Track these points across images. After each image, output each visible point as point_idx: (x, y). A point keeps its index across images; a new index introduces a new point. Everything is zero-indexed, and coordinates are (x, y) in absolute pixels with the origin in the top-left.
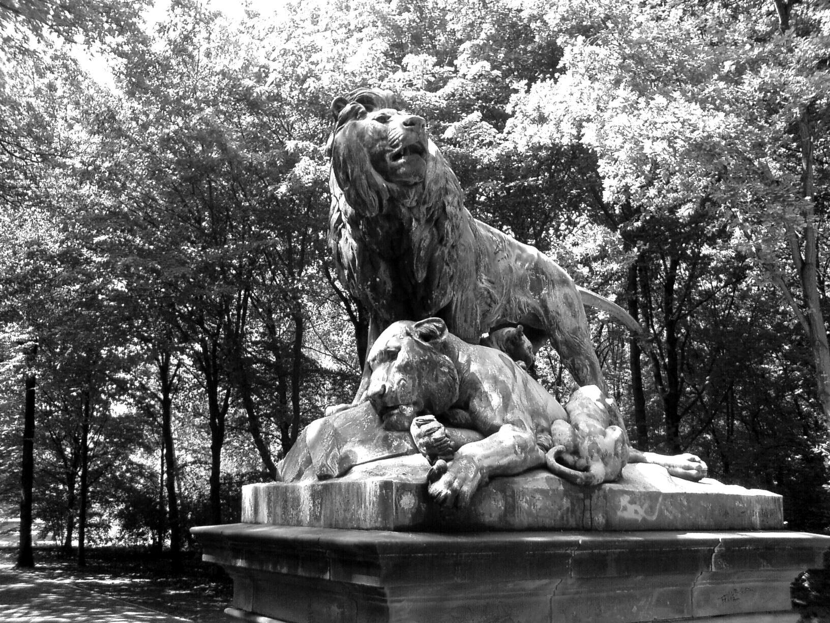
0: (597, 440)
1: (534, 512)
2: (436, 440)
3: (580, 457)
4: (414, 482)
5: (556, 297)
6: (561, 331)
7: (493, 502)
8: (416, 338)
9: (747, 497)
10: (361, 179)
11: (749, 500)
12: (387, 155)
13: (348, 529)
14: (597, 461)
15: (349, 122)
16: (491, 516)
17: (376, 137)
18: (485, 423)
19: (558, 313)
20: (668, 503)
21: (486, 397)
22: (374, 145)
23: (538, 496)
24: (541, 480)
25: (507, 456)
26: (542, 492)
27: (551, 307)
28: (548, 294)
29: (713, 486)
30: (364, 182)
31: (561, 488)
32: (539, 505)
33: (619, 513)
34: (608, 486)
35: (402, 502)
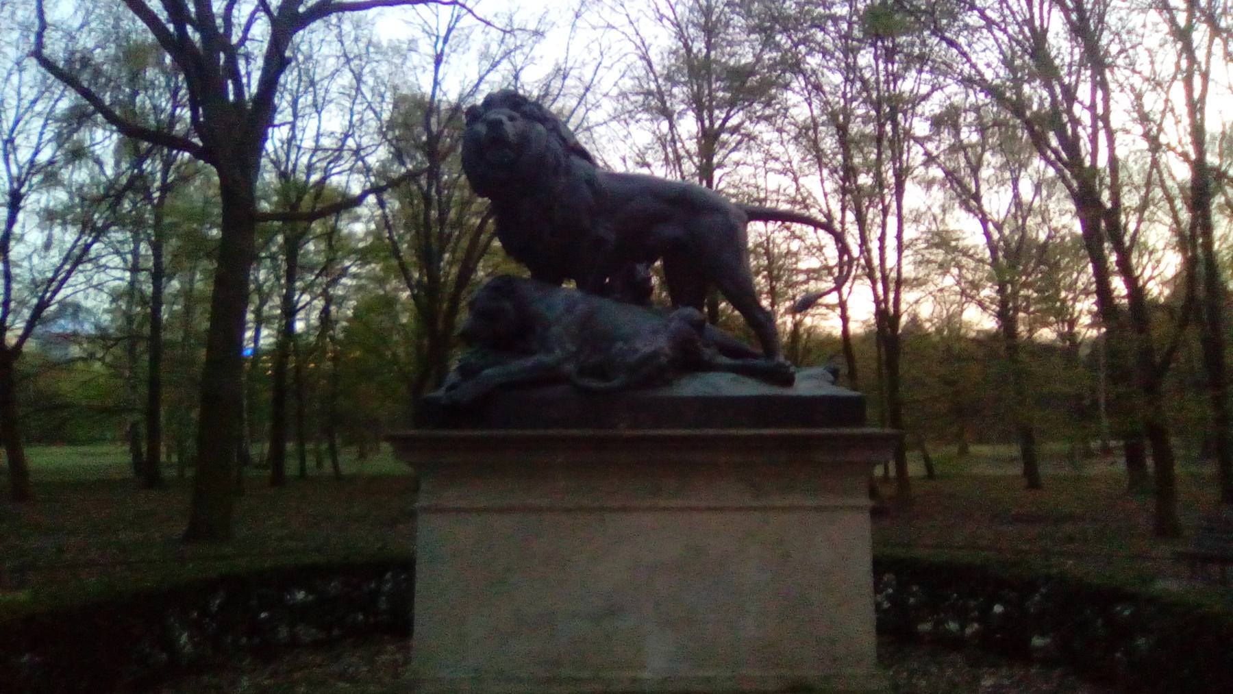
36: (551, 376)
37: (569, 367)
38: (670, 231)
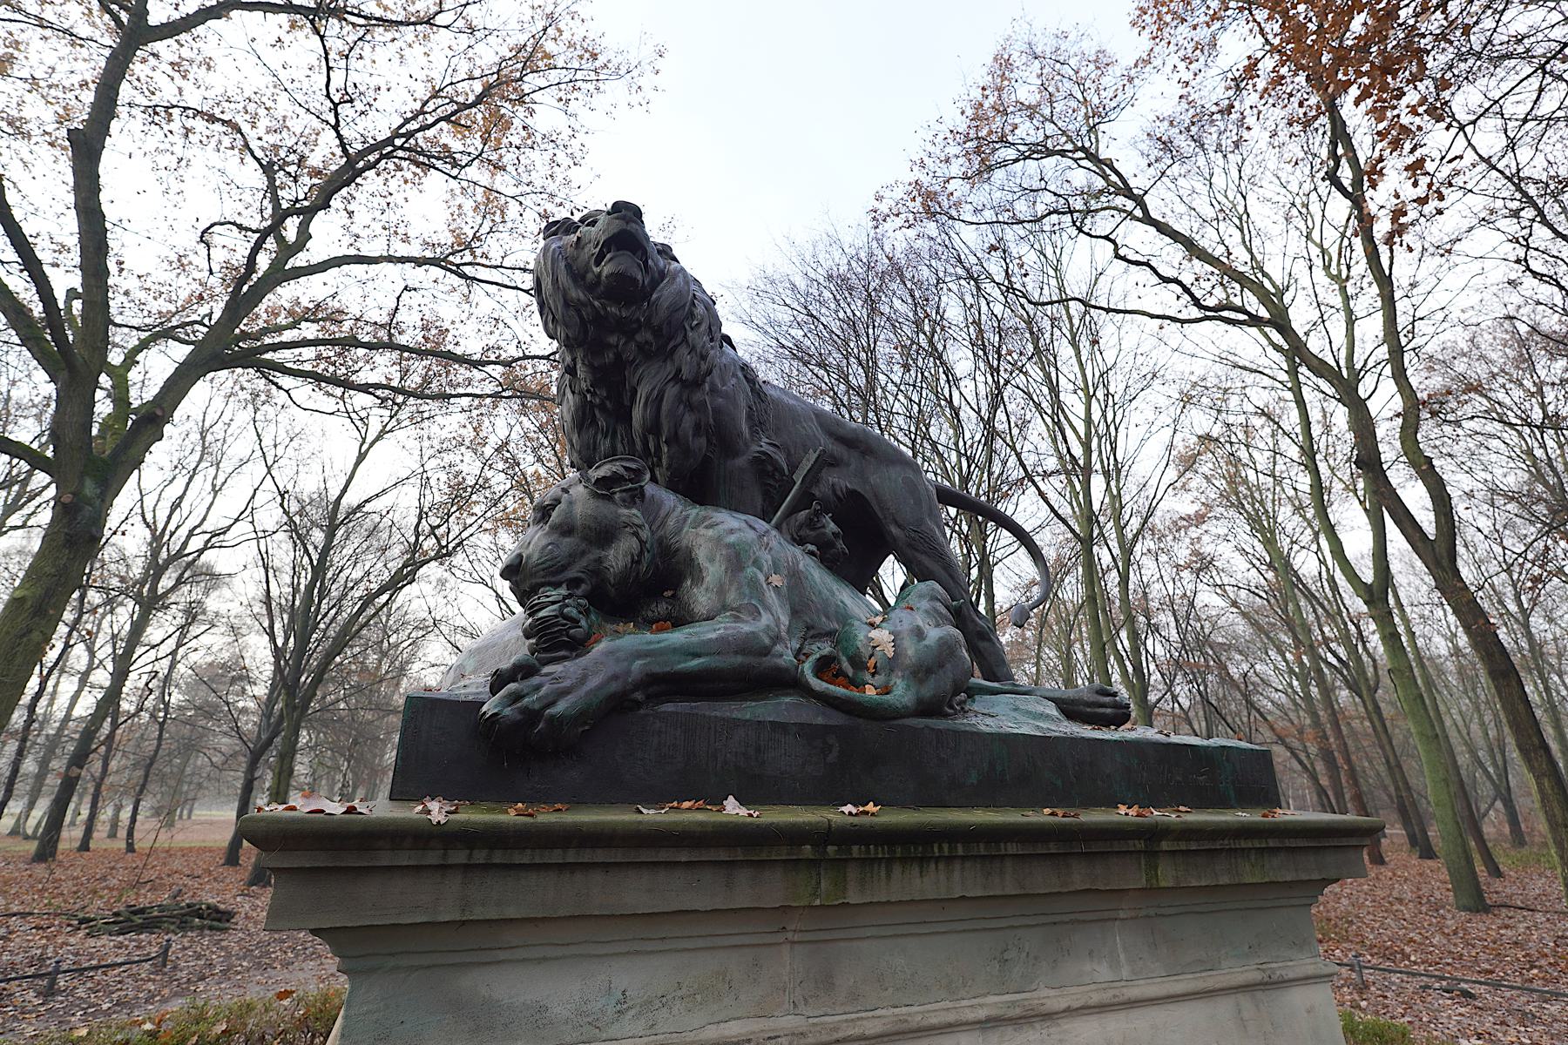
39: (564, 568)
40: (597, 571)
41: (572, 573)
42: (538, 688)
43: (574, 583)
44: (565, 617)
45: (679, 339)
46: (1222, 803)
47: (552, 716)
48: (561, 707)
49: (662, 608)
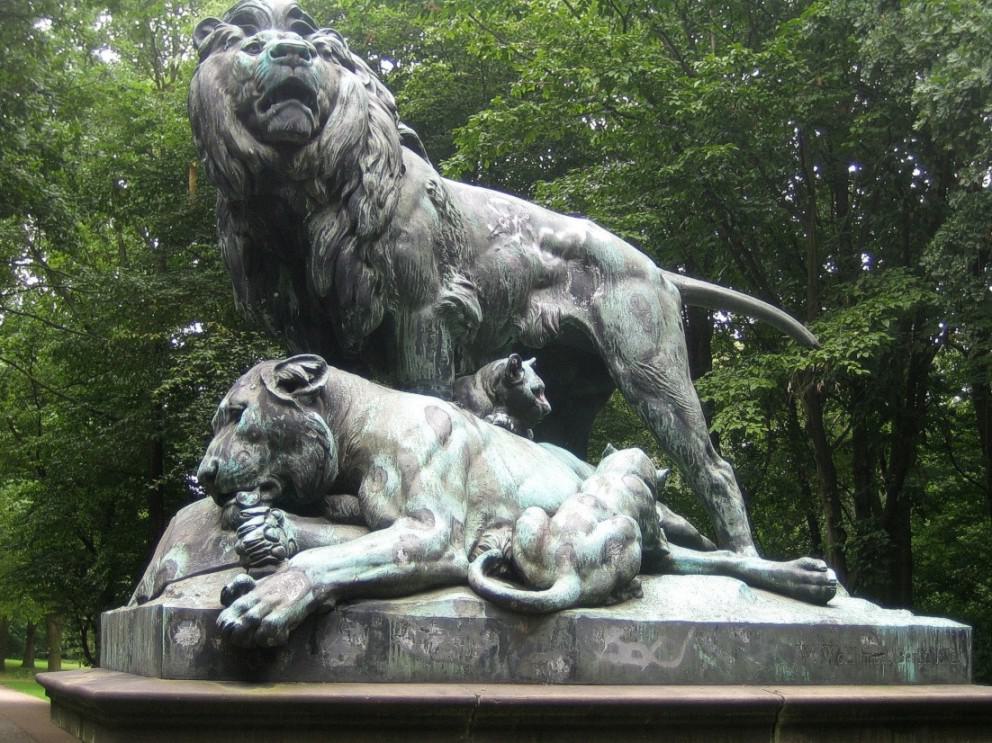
0: (575, 539)
1: (426, 652)
2: (248, 544)
3: (545, 567)
4: (201, 607)
5: (616, 302)
6: (624, 360)
7: (346, 638)
8: (272, 387)
9: (888, 629)
10: (217, 146)
11: (893, 634)
12: (256, 103)
13: (555, 684)
14: (568, 573)
15: (211, 57)
16: (340, 658)
17: (242, 77)
18: (373, 516)
19: (618, 328)
20: (707, 639)
21: (382, 476)
22: (239, 90)
23: (434, 629)
24: (446, 604)
25: (377, 565)
26: (445, 623)
27: (606, 318)
28: (604, 297)
29: (851, 610)
30: (223, 149)
31: (483, 616)
32: (436, 642)
33: (600, 656)
34: (579, 612)
35: (177, 636)
36: (427, 578)
37: (458, 558)
38: (550, 306)
39: (255, 474)
40: (286, 475)
41: (263, 479)
42: (257, 601)
43: (265, 487)
44: (268, 538)
45: (354, 182)
46: (898, 680)
47: (269, 624)
48: (273, 617)
49: (347, 502)
